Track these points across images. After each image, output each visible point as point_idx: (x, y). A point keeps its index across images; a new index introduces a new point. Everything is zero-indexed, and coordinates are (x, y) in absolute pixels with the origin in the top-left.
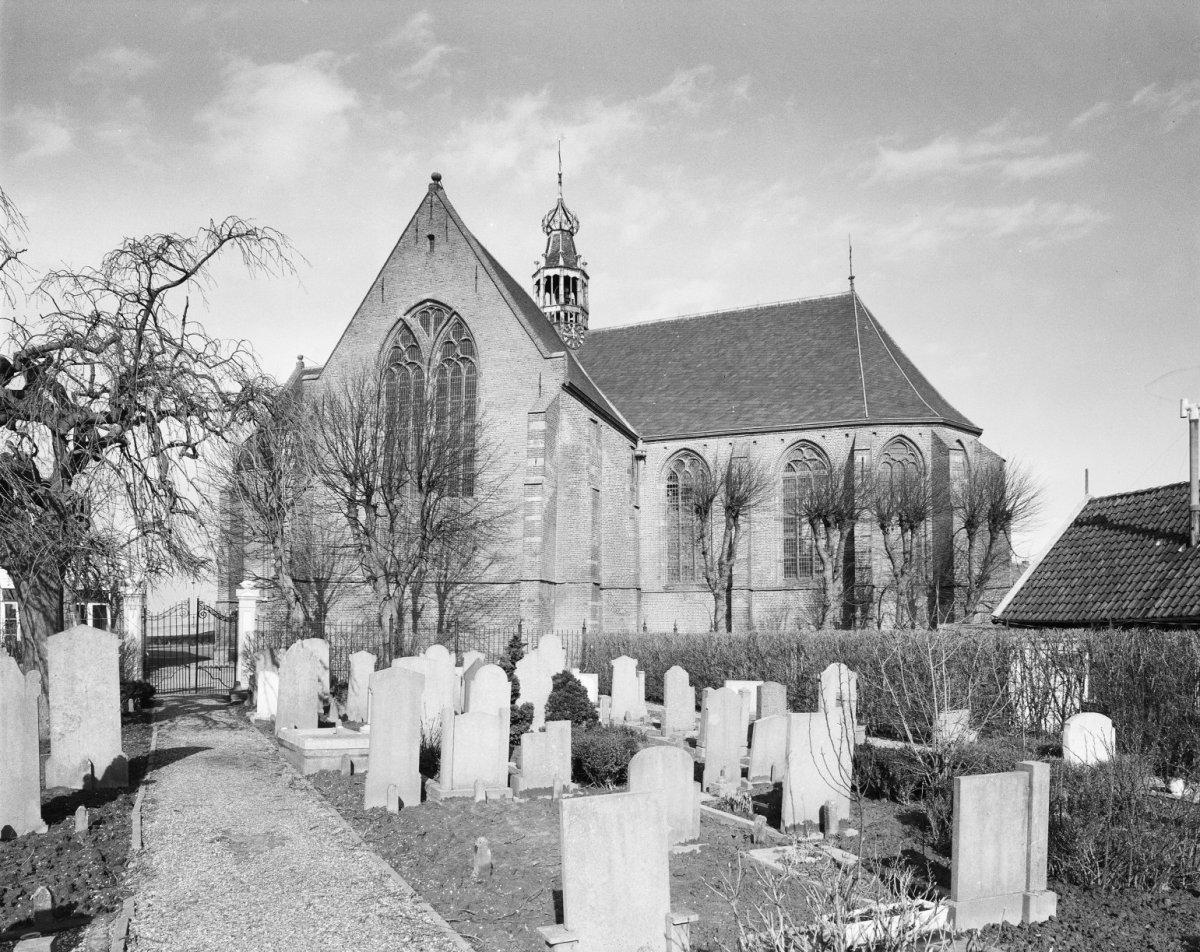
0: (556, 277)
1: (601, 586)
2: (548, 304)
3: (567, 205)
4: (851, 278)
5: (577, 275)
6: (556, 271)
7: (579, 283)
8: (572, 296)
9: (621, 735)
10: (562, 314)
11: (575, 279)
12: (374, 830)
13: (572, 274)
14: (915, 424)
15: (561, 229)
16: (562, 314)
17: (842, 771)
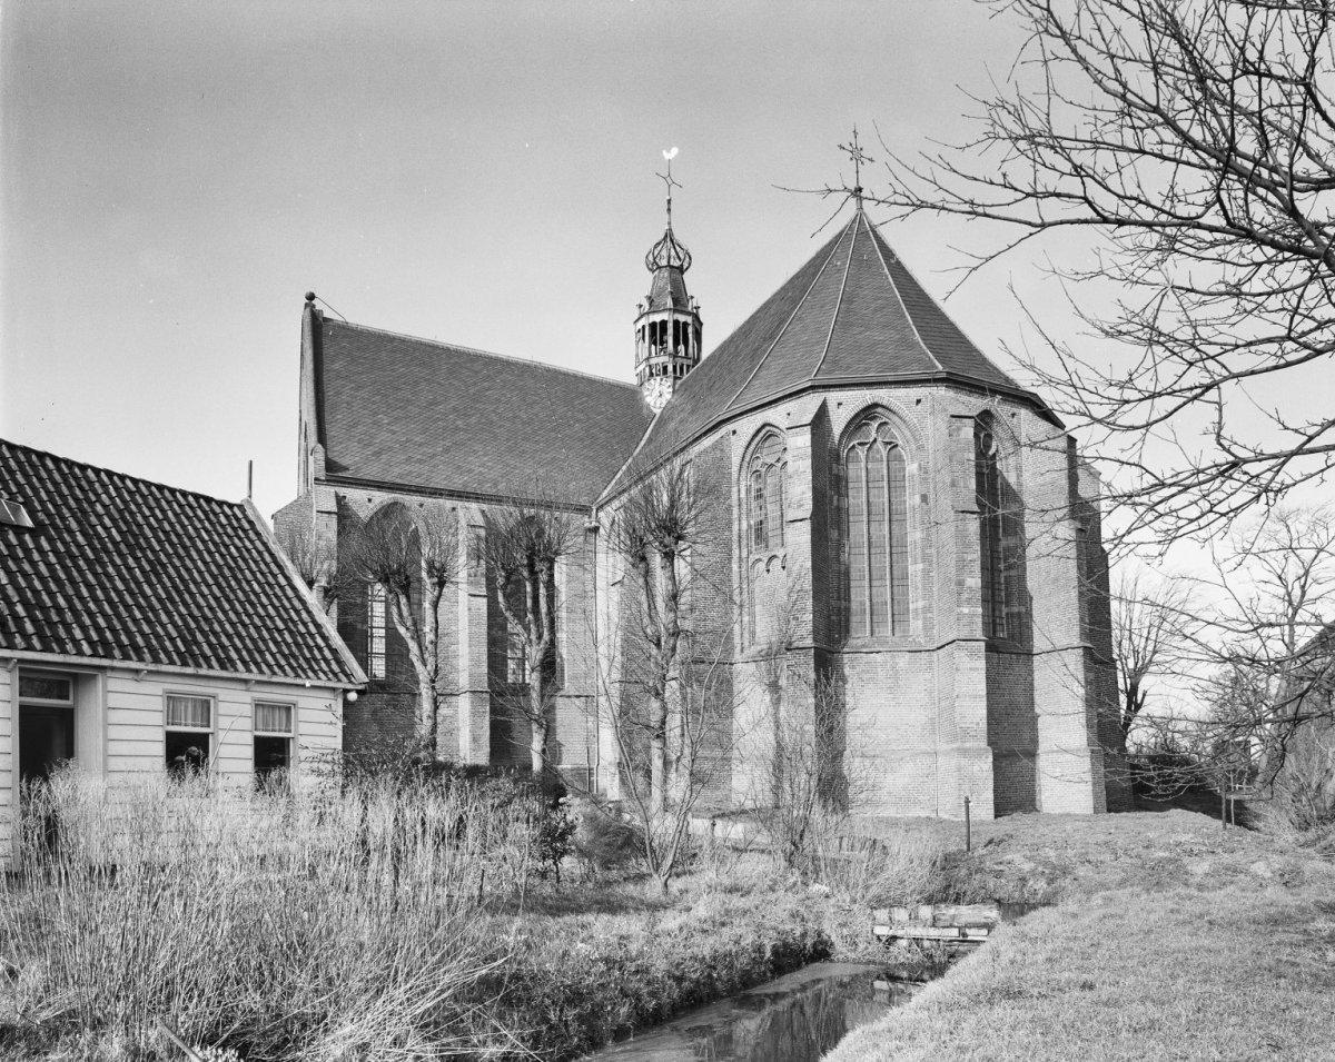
0: (664, 323)
1: (996, 840)
2: (654, 354)
3: (677, 236)
5: (689, 320)
6: (664, 316)
7: (690, 329)
8: (681, 348)
9: (829, 817)
11: (686, 324)
12: (402, 747)
13: (682, 318)
14: (734, 417)
15: (669, 266)
17: (1199, 391)
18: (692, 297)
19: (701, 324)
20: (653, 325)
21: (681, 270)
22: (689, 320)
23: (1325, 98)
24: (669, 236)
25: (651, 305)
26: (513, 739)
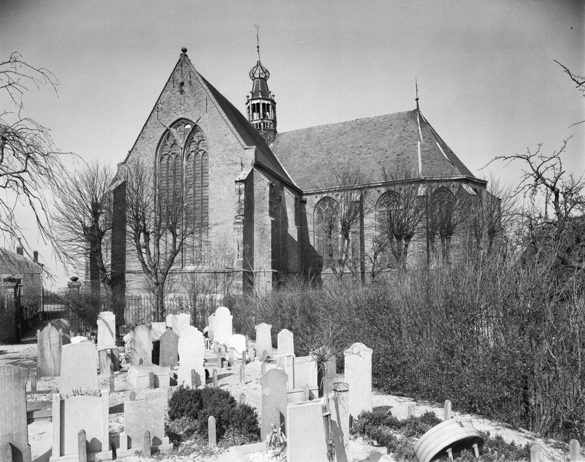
0: (258, 104)
4: (417, 99)
6: (258, 101)
10: (262, 124)
11: (268, 105)
13: (266, 102)
15: (260, 78)
16: (262, 124)
18: (271, 92)
19: (275, 103)
20: (254, 105)
21: (265, 80)
22: (270, 103)
23: (27, 252)
24: (259, 64)
25: (252, 96)
26: (123, 368)
